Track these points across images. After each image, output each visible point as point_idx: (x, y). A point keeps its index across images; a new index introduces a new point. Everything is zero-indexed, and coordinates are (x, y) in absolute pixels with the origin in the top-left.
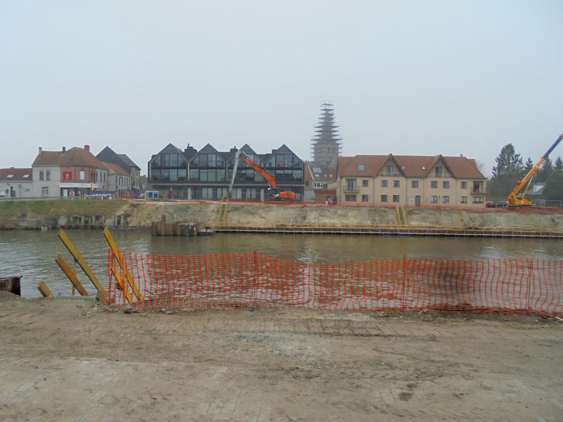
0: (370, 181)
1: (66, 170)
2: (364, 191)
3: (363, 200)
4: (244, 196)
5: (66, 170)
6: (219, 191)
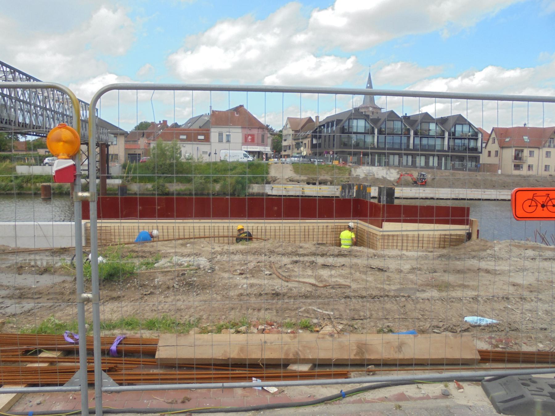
0: (536, 151)
1: (248, 132)
2: (530, 161)
3: (529, 169)
4: (427, 163)
5: (249, 132)
6: (405, 158)
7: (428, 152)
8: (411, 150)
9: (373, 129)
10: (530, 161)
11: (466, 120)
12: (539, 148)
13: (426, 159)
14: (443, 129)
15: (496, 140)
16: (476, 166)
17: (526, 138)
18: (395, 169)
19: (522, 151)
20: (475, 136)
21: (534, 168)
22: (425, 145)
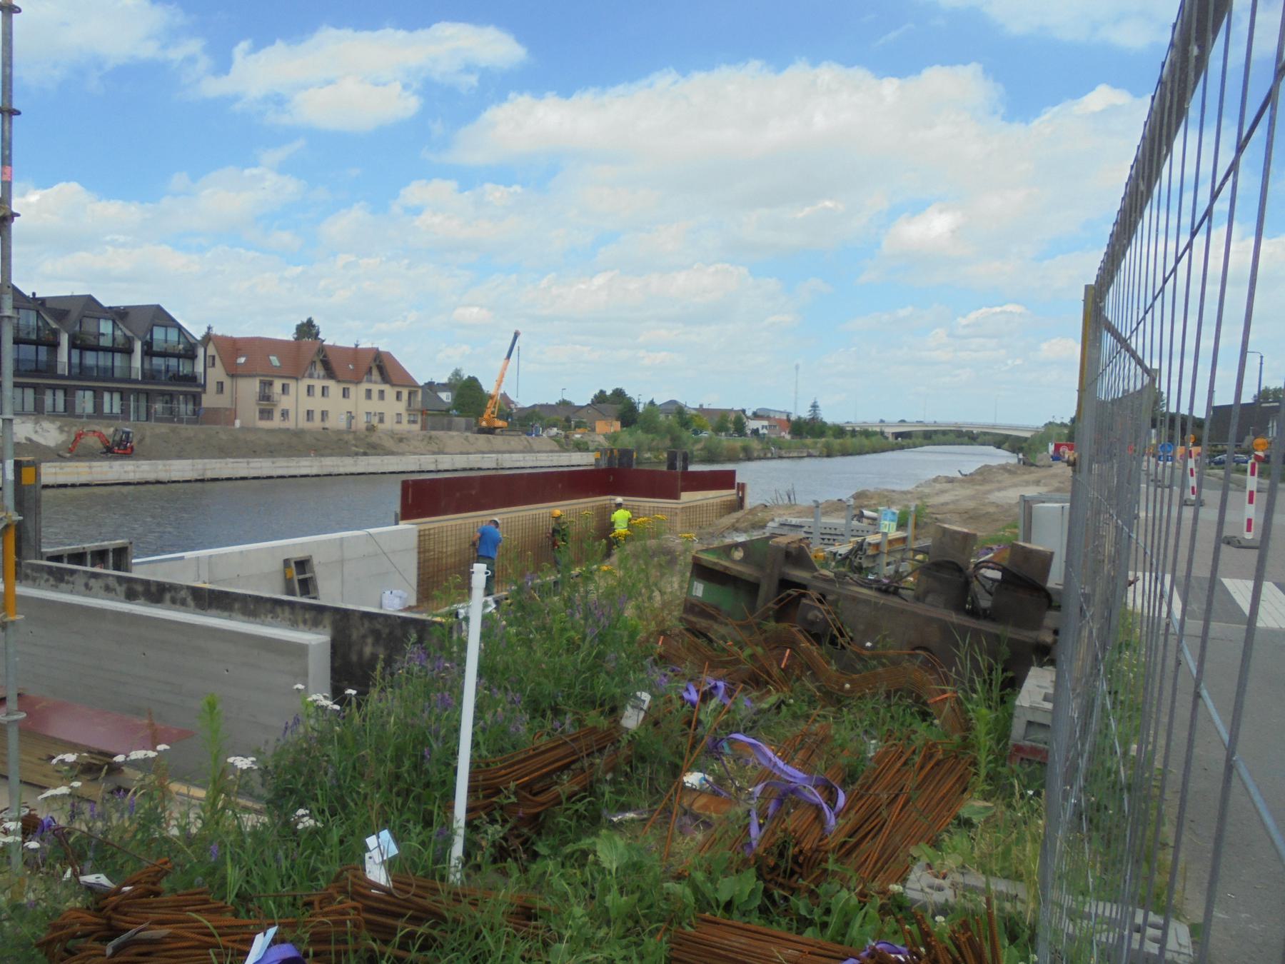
0: (352, 388)
4: (98, 406)
6: (49, 393)
7: (100, 381)
8: (62, 377)
9: (130, 341)
10: (285, 402)
11: (174, 320)
12: (297, 379)
13: (95, 397)
14: (129, 334)
15: (217, 359)
16: (195, 413)
17: (275, 360)
18: (53, 422)
19: (271, 384)
20: (189, 353)
21: (292, 415)
22: (91, 368)
